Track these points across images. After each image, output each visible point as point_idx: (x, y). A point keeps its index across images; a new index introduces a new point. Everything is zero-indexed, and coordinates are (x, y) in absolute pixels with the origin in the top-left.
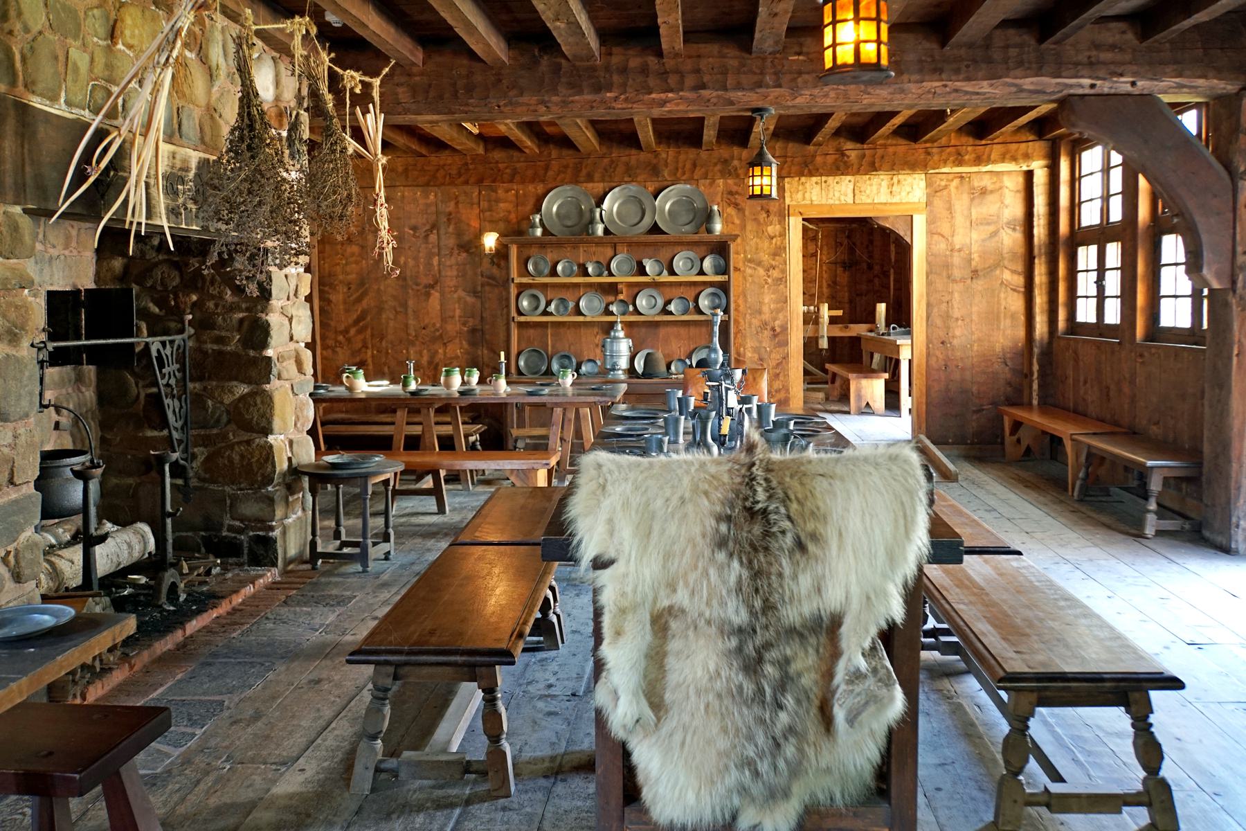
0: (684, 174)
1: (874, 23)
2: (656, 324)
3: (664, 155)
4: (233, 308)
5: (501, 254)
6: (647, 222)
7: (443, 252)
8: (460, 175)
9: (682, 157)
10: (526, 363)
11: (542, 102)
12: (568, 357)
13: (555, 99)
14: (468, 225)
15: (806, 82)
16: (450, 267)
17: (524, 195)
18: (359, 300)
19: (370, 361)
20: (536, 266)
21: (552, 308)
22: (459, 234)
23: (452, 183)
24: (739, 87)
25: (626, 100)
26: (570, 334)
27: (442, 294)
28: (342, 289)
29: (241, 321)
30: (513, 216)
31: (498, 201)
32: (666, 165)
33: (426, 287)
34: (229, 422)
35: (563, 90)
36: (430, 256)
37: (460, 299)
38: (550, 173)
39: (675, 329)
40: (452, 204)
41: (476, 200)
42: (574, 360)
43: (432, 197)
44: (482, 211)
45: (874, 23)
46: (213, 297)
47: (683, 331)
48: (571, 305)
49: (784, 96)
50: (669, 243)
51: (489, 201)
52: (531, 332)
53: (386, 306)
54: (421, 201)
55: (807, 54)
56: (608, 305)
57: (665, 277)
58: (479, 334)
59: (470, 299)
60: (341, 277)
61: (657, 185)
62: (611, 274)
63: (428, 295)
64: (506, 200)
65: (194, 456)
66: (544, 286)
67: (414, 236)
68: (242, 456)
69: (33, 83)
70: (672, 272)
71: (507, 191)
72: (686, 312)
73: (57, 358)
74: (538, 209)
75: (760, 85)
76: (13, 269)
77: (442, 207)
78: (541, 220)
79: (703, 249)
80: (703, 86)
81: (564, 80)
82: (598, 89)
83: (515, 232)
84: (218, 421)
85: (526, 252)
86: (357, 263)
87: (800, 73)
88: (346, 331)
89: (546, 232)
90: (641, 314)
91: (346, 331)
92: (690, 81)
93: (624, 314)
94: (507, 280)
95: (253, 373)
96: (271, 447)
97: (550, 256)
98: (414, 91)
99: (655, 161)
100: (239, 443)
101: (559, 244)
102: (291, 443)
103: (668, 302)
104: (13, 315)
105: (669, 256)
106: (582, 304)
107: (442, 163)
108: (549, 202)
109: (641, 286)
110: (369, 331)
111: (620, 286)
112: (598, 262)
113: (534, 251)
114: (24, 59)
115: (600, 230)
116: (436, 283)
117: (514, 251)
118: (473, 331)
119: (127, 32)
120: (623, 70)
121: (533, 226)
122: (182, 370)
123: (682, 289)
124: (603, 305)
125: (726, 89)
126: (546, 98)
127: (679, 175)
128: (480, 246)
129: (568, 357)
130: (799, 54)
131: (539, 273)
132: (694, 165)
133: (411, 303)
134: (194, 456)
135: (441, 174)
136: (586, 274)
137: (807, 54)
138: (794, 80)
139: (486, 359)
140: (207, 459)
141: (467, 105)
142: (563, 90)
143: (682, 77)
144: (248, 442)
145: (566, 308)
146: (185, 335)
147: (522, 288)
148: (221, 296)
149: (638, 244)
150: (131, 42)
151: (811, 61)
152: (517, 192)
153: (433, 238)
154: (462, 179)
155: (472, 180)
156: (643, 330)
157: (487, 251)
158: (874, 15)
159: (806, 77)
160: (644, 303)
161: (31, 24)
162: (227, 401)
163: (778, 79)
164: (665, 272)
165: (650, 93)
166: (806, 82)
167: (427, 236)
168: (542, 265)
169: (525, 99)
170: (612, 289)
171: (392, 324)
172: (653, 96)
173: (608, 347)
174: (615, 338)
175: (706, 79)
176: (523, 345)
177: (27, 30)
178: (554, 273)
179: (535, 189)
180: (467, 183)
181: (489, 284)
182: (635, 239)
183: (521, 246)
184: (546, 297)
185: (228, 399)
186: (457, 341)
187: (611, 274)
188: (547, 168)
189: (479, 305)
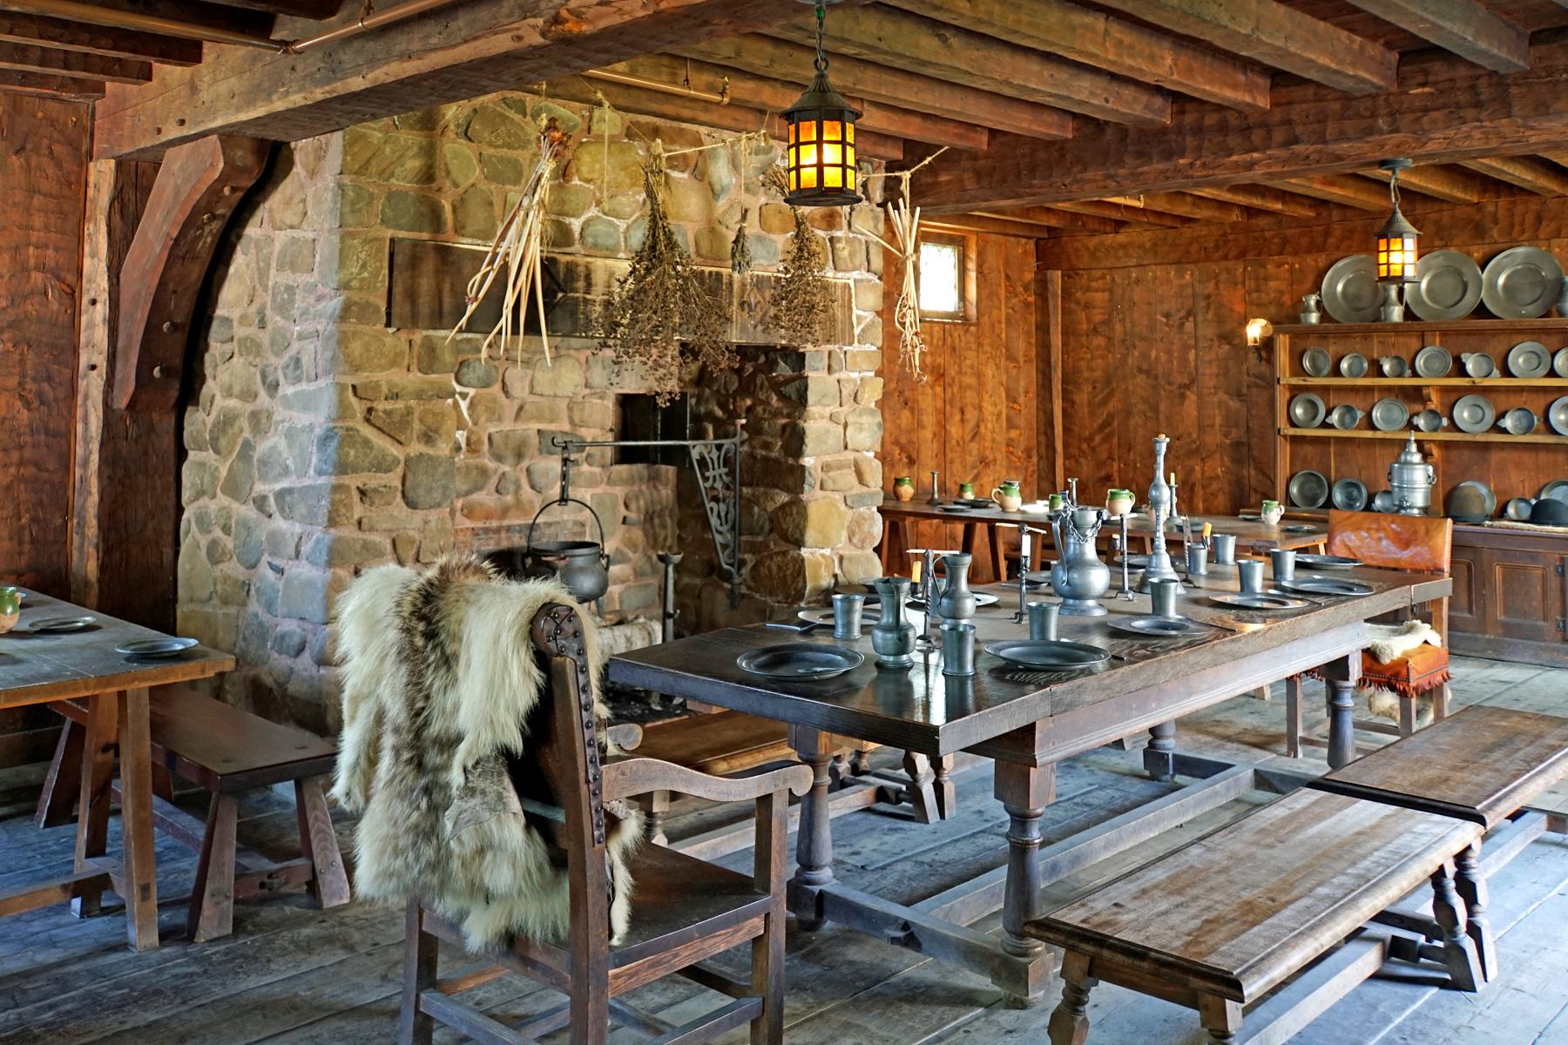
0: (1523, 232)
1: (839, 147)
2: (1486, 446)
3: (1491, 208)
4: (776, 414)
5: (1267, 344)
6: (1469, 302)
7: (1201, 345)
8: (1217, 247)
9: (1520, 209)
10: (1301, 489)
11: (1111, 177)
12: (1356, 486)
13: (1121, 171)
14: (1231, 310)
15: (1434, 122)
16: (1208, 361)
17: (1301, 269)
18: (1105, 402)
19: (1116, 475)
20: (1313, 361)
21: (1335, 417)
22: (1220, 321)
23: (1208, 259)
24: (1342, 137)
25: (1204, 165)
26: (1360, 455)
27: (1200, 396)
28: (1087, 388)
29: (784, 427)
30: (1286, 298)
31: (1266, 279)
32: (1496, 221)
33: (1180, 387)
34: (771, 531)
35: (1130, 161)
36: (1185, 348)
37: (1220, 402)
38: (1331, 240)
39: (1515, 455)
40: (1211, 285)
41: (1240, 279)
42: (1364, 490)
43: (1188, 277)
44: (1249, 292)
45: (839, 147)
46: (762, 402)
47: (1527, 458)
48: (1360, 414)
49: (1406, 142)
50: (1502, 331)
51: (1257, 279)
52: (1308, 450)
53: (1135, 410)
54: (1176, 282)
55: (1435, 84)
56: (1411, 417)
57: (1497, 380)
58: (1244, 449)
59: (1234, 404)
60: (1086, 374)
61: (1487, 249)
62: (1415, 374)
63: (1183, 397)
64: (1277, 276)
65: (742, 563)
66: (1324, 390)
67: (1167, 324)
68: (779, 568)
69: (463, 227)
70: (1506, 373)
71: (1279, 266)
72: (1528, 429)
73: (625, 456)
74: (1317, 288)
75: (1371, 131)
76: (431, 383)
77: (1199, 289)
78: (1318, 303)
79: (1555, 340)
80: (1296, 141)
81: (1130, 148)
82: (1169, 155)
83: (1286, 319)
84: (762, 528)
85: (1301, 345)
86: (1103, 357)
87: (1426, 110)
88: (1090, 439)
89: (1325, 317)
90: (1460, 430)
91: (1090, 439)
92: (1279, 135)
93: (1435, 430)
94: (1270, 383)
95: (790, 481)
96: (803, 560)
97: (1333, 349)
98: (978, 175)
99: (1478, 217)
100: (777, 554)
101: (1345, 334)
102: (841, 559)
103: (1502, 415)
104: (430, 420)
105: (1502, 349)
106: (1376, 414)
107: (1196, 234)
108: (1332, 278)
109: (1460, 392)
110: (1115, 440)
111: (1425, 391)
112: (1397, 357)
113: (1312, 344)
114: (454, 210)
115: (1396, 313)
116: (1192, 382)
117: (1283, 342)
118: (1237, 445)
119: (584, 169)
120: (1198, 130)
121: (1307, 310)
122: (731, 473)
123: (1524, 397)
124: (1406, 417)
125: (1325, 142)
126: (1112, 171)
127: (1515, 234)
128: (1244, 337)
129: (1356, 486)
130: (1424, 85)
131: (1317, 372)
132: (1539, 219)
133: (1163, 407)
134: (742, 563)
135: (1195, 247)
136: (1381, 374)
137: (1435, 84)
138: (1418, 120)
139: (1253, 483)
140: (754, 568)
141: (1031, 186)
142: (1130, 161)
143: (1269, 132)
144: (784, 553)
145: (1354, 419)
146: (737, 440)
147: (1295, 391)
148: (767, 403)
149: (1458, 333)
150: (589, 176)
151: (1442, 92)
152: (1292, 266)
153: (1189, 325)
154: (1220, 253)
155: (1233, 253)
156: (1466, 454)
157: (1250, 343)
158: (814, 138)
159: (1435, 114)
160: (1466, 414)
161: (460, 179)
162: (770, 509)
163: (1395, 121)
164: (1496, 372)
165: (1230, 156)
166: (1434, 122)
167: (1182, 325)
168: (1321, 361)
169: (1089, 175)
170: (1415, 395)
171: (1141, 432)
172: (1234, 158)
173: (1395, 474)
174: (1407, 463)
175: (1299, 130)
176: (1298, 464)
177: (456, 185)
178: (1336, 372)
179: (1313, 261)
180: (1225, 258)
181: (1257, 385)
182: (1455, 326)
183: (1295, 337)
184: (1327, 404)
185: (771, 507)
186: (1218, 456)
187: (1415, 374)
188: (1327, 234)
189: (1245, 410)
